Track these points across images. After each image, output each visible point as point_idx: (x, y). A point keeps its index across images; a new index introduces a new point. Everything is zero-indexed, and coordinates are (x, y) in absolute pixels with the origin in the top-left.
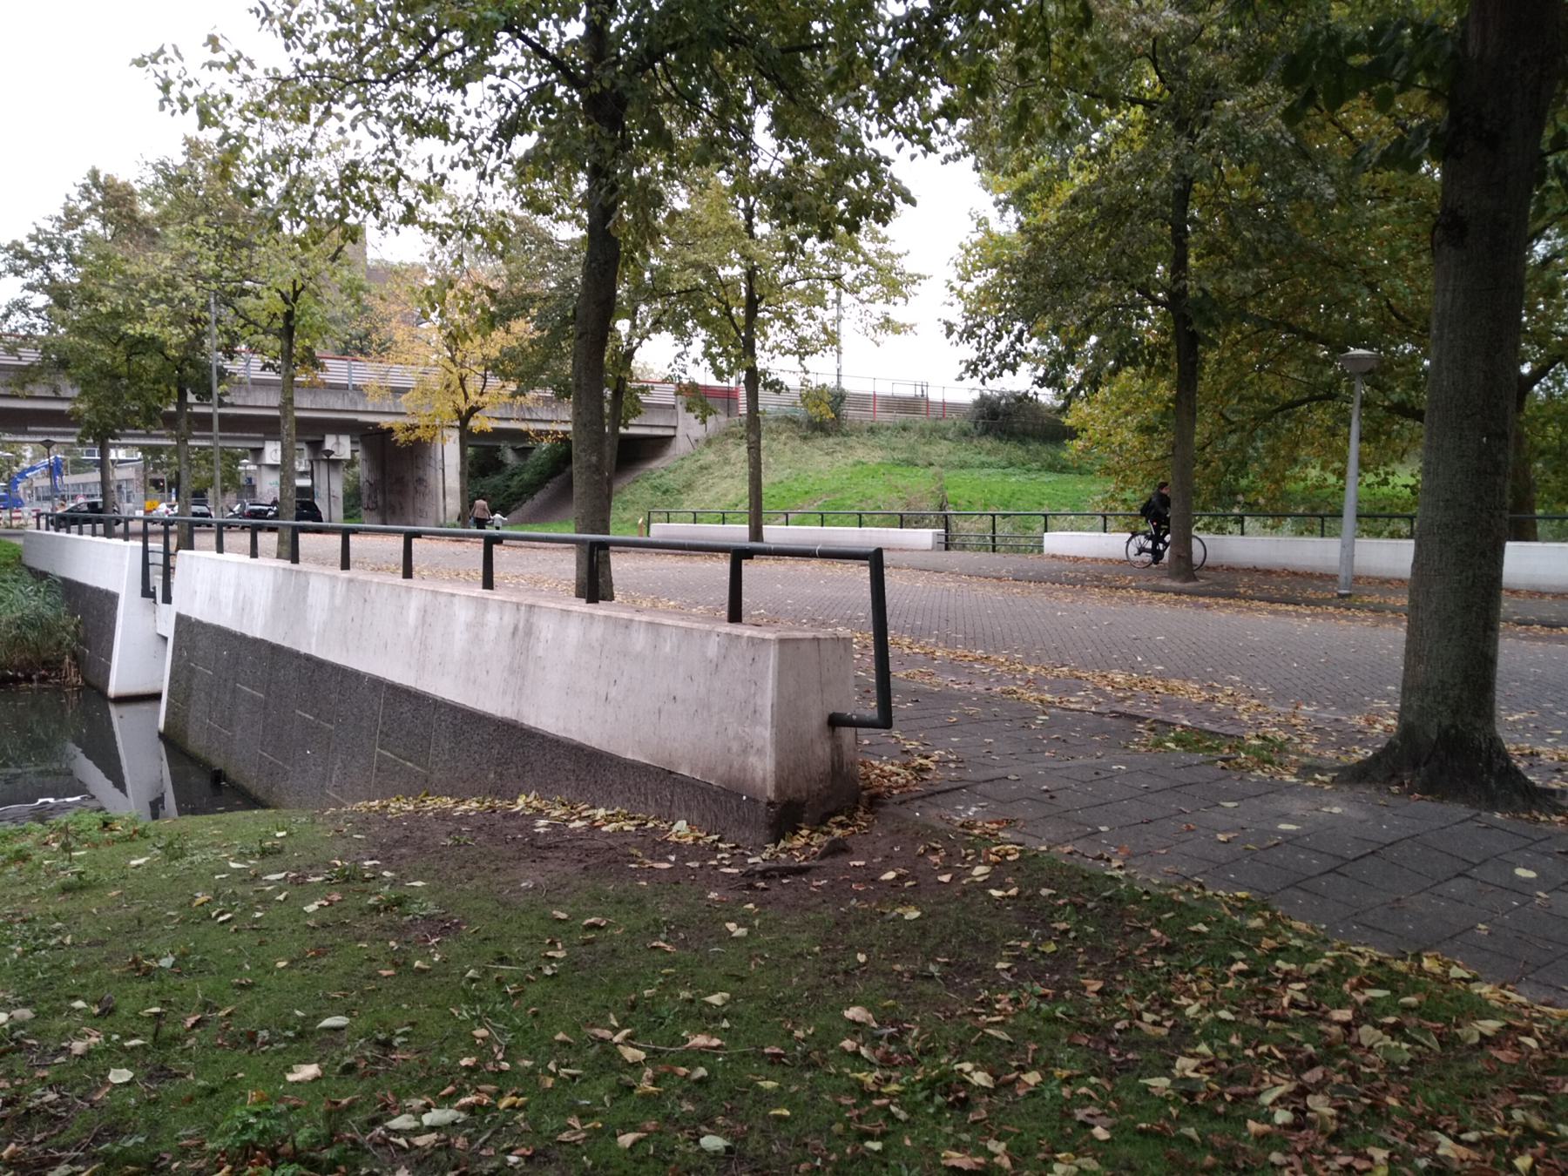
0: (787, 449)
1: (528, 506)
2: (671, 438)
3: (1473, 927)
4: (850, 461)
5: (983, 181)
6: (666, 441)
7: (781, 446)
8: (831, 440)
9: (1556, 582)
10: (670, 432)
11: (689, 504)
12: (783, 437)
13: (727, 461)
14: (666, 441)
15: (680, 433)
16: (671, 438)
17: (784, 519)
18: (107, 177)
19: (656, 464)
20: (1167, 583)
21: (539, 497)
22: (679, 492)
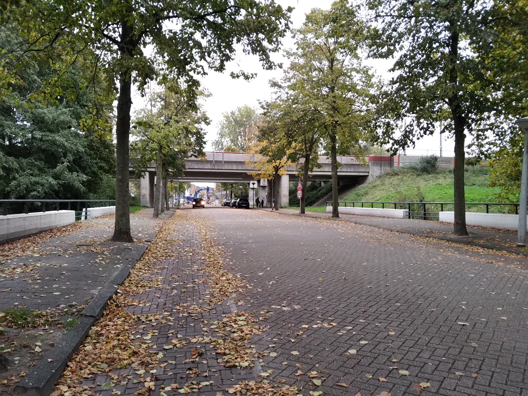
0: (409, 179)
1: (317, 203)
2: (367, 176)
3: (373, 376)
4: (434, 184)
5: (248, 113)
6: (366, 177)
7: (407, 178)
8: (430, 176)
9: (375, 213)
10: (367, 174)
11: (369, 198)
12: (408, 175)
13: (383, 184)
14: (366, 177)
15: (370, 174)
16: (367, 176)
17: (352, 205)
18: (240, 110)
19: (360, 187)
20: (84, 214)
21: (325, 197)
22: (363, 196)
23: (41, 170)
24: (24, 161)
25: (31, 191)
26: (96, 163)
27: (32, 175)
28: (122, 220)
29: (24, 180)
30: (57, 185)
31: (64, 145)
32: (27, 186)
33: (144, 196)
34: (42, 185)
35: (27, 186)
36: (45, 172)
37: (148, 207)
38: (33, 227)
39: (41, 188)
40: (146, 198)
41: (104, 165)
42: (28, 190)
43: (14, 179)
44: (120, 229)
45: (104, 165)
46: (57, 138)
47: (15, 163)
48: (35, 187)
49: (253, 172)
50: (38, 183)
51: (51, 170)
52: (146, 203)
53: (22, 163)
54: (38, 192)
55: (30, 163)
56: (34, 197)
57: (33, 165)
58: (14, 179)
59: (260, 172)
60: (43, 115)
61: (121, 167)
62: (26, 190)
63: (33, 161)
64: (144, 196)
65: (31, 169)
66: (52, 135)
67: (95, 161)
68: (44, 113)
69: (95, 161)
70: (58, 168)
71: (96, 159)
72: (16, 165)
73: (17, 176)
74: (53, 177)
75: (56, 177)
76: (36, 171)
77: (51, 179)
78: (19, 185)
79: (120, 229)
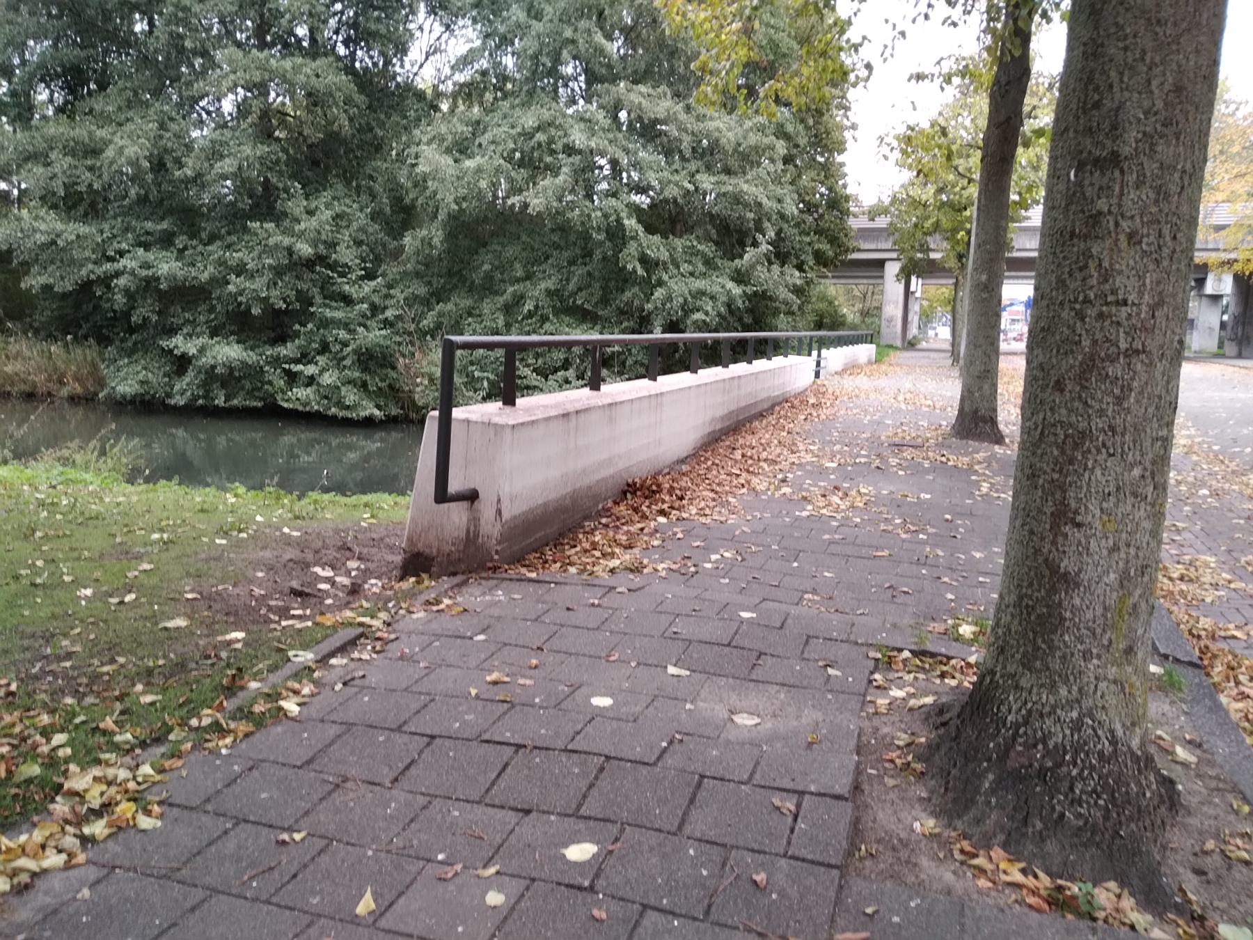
23: (708, 262)
24: (679, 243)
25: (692, 311)
26: (810, 244)
27: (692, 274)
28: (980, 389)
29: (677, 287)
30: (741, 297)
31: (760, 205)
32: (685, 300)
33: (890, 321)
34: (713, 298)
35: (685, 300)
36: (716, 268)
37: (897, 348)
38: (763, 395)
39: (711, 303)
40: (895, 326)
41: (824, 246)
42: (687, 310)
43: (660, 283)
44: (976, 411)
45: (824, 246)
46: (745, 187)
47: (662, 248)
48: (698, 303)
49: (1213, 255)
50: (702, 293)
51: (728, 263)
52: (894, 338)
53: (674, 249)
54: (707, 314)
55: (689, 248)
56: (703, 326)
57: (695, 253)
58: (660, 283)
59: (1233, 256)
60: (717, 134)
61: (989, 252)
62: (683, 309)
63: (695, 243)
64: (890, 321)
65: (690, 262)
66: (732, 181)
67: (808, 239)
68: (718, 129)
69: (808, 239)
70: (746, 257)
71: (808, 234)
72: (664, 255)
73: (665, 277)
74: (733, 279)
75: (740, 278)
76: (701, 267)
77: (730, 285)
78: (669, 298)
79: (976, 411)
